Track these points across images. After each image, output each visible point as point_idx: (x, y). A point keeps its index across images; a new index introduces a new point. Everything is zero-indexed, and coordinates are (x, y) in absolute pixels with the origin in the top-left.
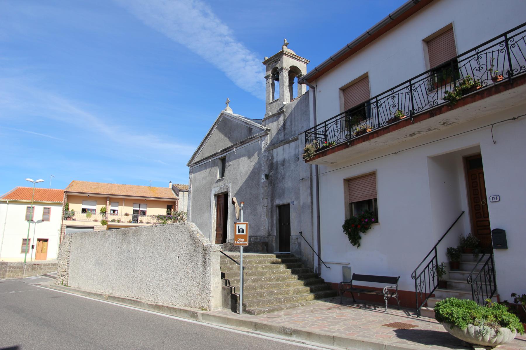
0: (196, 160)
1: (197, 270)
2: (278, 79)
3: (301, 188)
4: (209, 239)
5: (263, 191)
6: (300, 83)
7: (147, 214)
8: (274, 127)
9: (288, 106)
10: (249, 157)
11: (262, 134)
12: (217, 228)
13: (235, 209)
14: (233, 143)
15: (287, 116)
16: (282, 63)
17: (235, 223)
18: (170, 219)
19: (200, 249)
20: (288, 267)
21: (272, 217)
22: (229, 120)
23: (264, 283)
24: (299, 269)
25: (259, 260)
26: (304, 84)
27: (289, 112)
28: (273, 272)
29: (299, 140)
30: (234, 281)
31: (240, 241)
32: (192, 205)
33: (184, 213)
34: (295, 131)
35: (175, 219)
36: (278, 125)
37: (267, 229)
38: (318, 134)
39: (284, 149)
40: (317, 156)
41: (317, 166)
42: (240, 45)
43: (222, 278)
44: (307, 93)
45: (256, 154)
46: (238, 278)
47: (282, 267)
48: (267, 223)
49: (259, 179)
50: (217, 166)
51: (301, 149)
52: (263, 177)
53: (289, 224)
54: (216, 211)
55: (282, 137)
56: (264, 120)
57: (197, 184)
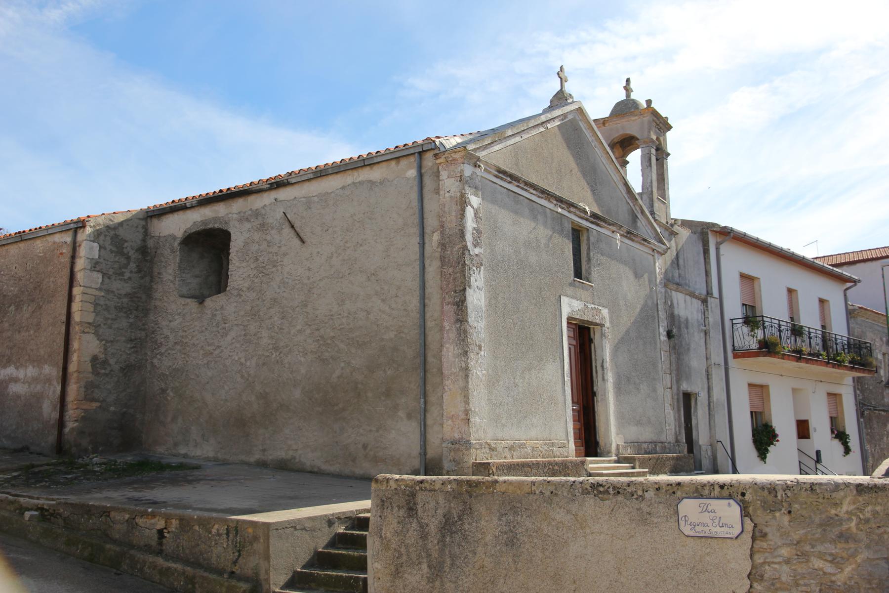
21: (679, 410)
48: (672, 418)
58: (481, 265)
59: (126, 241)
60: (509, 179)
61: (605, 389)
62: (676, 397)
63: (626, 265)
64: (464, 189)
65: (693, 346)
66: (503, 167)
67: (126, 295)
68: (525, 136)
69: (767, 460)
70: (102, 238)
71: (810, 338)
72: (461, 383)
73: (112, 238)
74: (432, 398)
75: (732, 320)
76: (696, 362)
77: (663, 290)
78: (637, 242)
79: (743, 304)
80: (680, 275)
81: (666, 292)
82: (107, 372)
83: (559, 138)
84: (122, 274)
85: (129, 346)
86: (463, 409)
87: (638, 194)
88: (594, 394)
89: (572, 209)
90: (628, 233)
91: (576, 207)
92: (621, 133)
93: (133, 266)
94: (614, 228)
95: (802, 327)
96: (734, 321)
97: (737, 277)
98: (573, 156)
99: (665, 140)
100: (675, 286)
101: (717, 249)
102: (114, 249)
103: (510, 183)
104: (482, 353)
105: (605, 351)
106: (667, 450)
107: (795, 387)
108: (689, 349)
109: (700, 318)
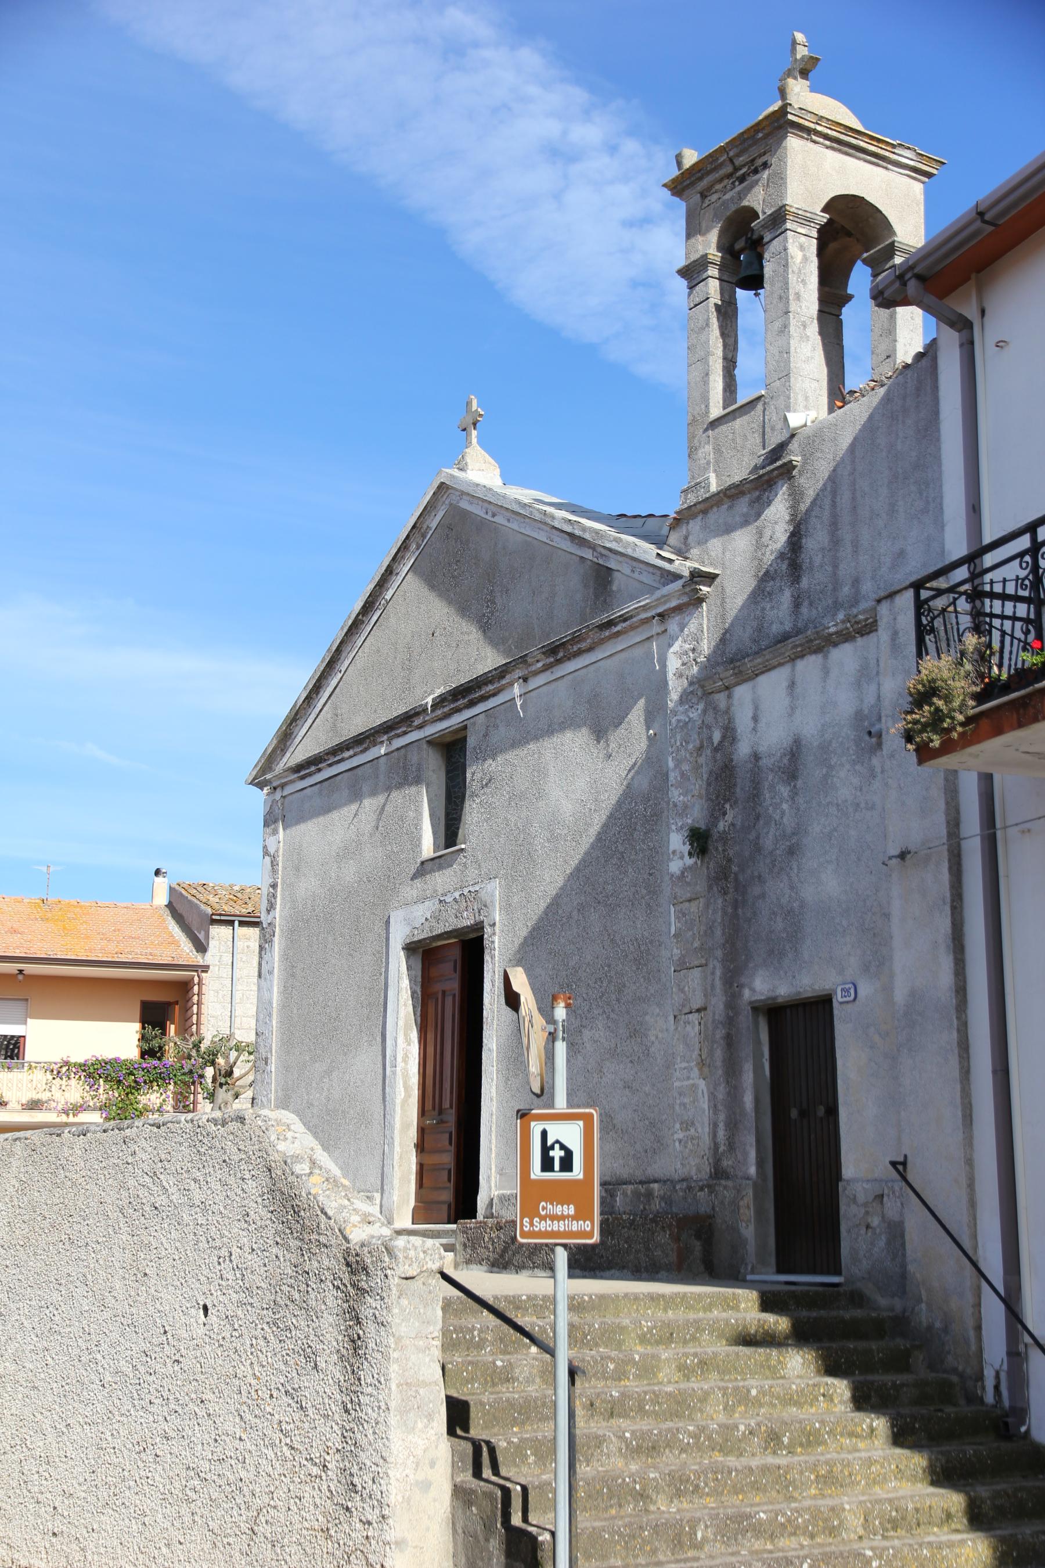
0: (300, 751)
1: (311, 1386)
2: (754, 282)
3: (896, 908)
4: (377, 1199)
5: (676, 921)
6: (887, 299)
7: (31, 1053)
8: (736, 558)
9: (817, 436)
10: (600, 733)
11: (667, 598)
12: (422, 1131)
13: (521, 1039)
14: (507, 652)
15: (810, 494)
16: (780, 180)
17: (523, 1115)
18: (160, 1079)
19: (329, 1262)
20: (832, 1368)
21: (732, 1070)
22: (482, 525)
23: (693, 1464)
24: (900, 1379)
25: (668, 1325)
26: (906, 302)
27: (823, 468)
28: (743, 1398)
29: (883, 634)
30: (519, 1450)
31: (554, 1218)
32: (284, 1007)
33: (238, 1048)
34: (856, 582)
35: (186, 1085)
36: (759, 545)
37: (706, 1140)
38: (992, 595)
39: (792, 685)
40: (984, 725)
41: (987, 780)
42: (530, 57)
43: (451, 1432)
44: (928, 355)
45: (636, 715)
46: (544, 1430)
47: (798, 1364)
49: (657, 854)
50: (417, 781)
51: (894, 686)
52: (677, 842)
53: (833, 1111)
54: (414, 1035)
55: (780, 614)
56: (677, 522)
57: (308, 885)
60: (313, 768)
89: (417, 722)
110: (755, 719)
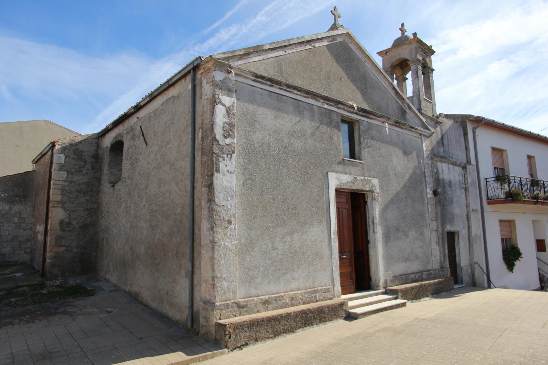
21: (443, 245)
37: (439, 260)
48: (438, 252)
58: (233, 152)
59: (84, 152)
60: (269, 83)
61: (375, 239)
62: (441, 237)
63: (396, 146)
64: (214, 91)
65: (455, 199)
66: (261, 73)
67: (84, 183)
68: (289, 51)
69: (514, 271)
70: (67, 151)
71: (544, 188)
72: (210, 253)
73: (74, 151)
74: (196, 263)
75: (486, 179)
76: (457, 210)
77: (430, 162)
78: (406, 129)
79: (495, 168)
80: (444, 151)
81: (432, 163)
82: (71, 229)
83: (328, 54)
84: (81, 171)
85: (86, 213)
86: (211, 275)
87: (408, 98)
88: (368, 242)
89: (340, 106)
90: (397, 122)
91: (344, 104)
92: (398, 58)
93: (89, 166)
94: (384, 120)
95: (538, 181)
96: (488, 180)
97: (490, 150)
98: (343, 68)
99: (430, 60)
100: (440, 159)
101: (474, 132)
102: (76, 157)
103: (271, 86)
104: (233, 227)
105: (376, 210)
106: (433, 276)
107: (534, 219)
108: (452, 202)
109: (461, 179)
110: (442, 171)
